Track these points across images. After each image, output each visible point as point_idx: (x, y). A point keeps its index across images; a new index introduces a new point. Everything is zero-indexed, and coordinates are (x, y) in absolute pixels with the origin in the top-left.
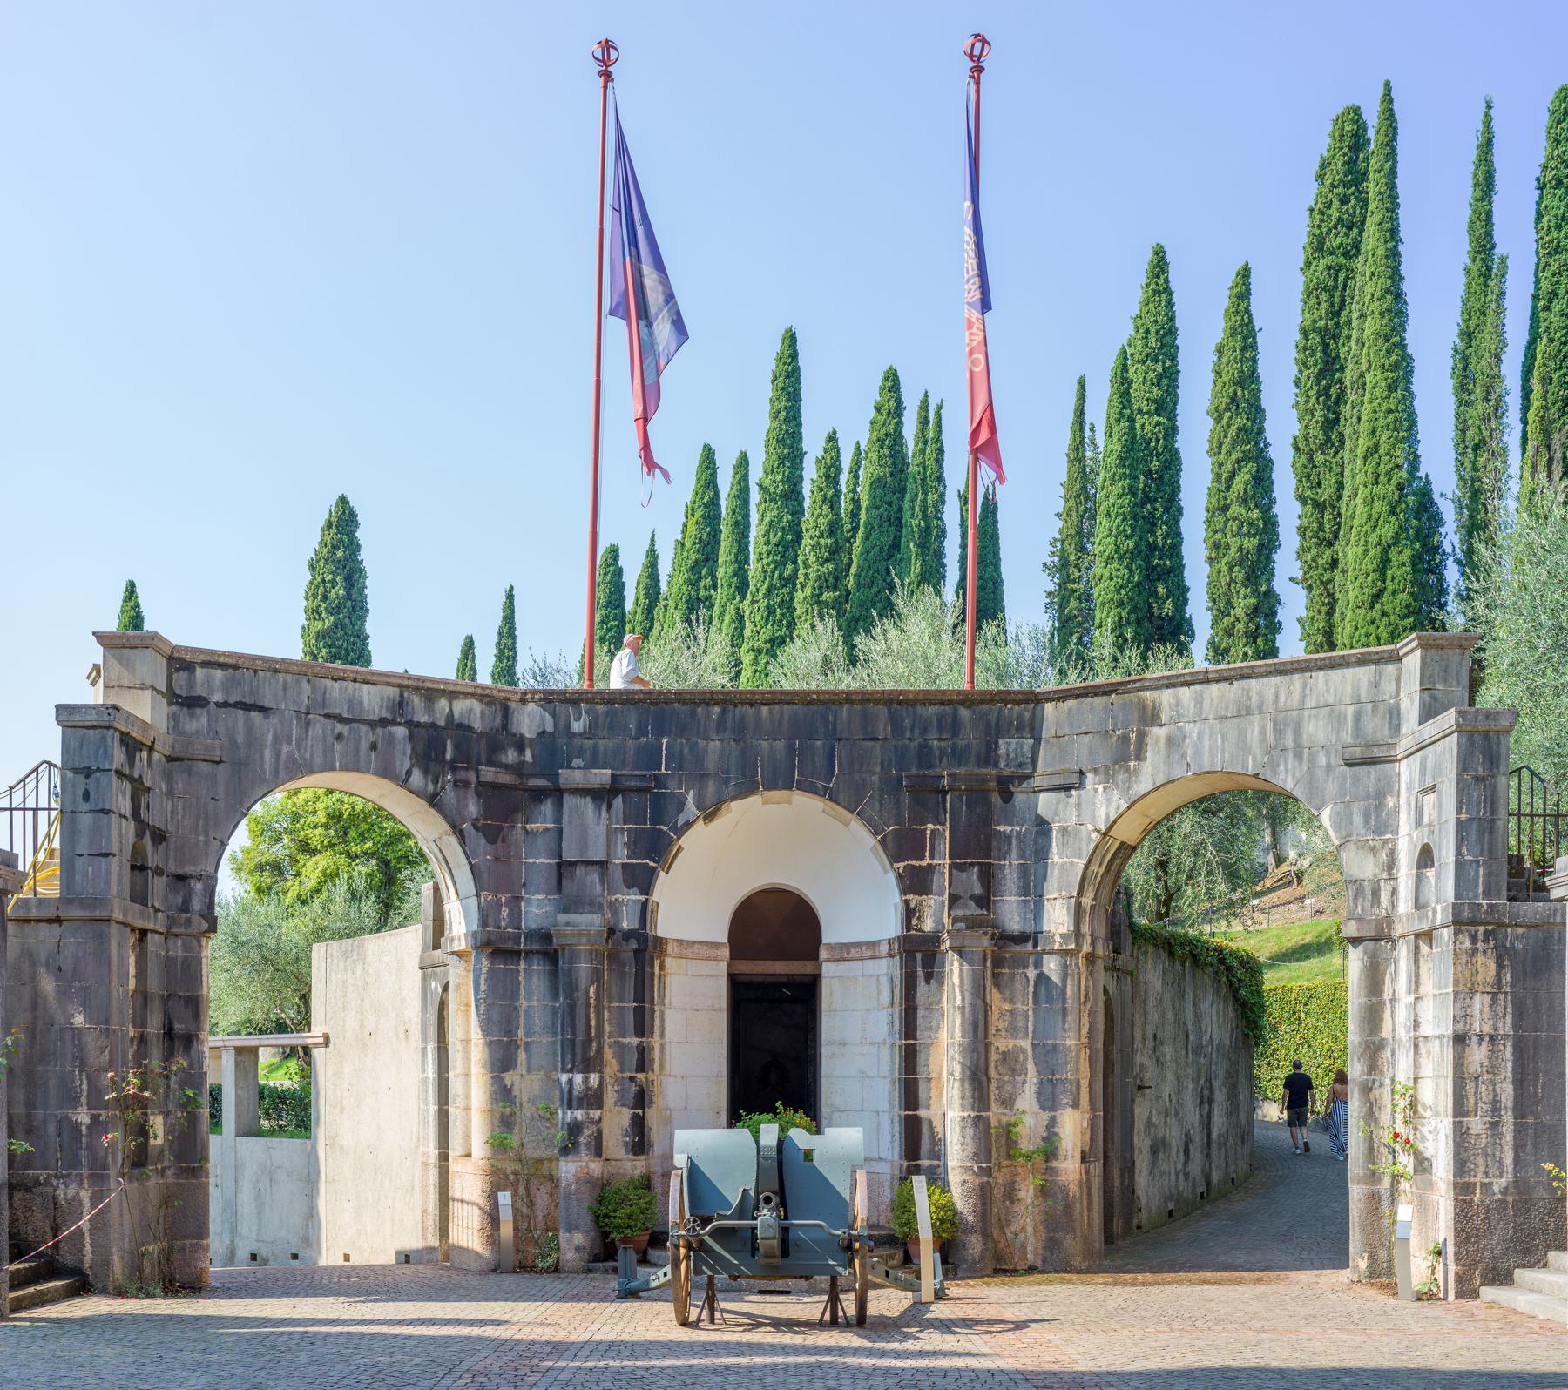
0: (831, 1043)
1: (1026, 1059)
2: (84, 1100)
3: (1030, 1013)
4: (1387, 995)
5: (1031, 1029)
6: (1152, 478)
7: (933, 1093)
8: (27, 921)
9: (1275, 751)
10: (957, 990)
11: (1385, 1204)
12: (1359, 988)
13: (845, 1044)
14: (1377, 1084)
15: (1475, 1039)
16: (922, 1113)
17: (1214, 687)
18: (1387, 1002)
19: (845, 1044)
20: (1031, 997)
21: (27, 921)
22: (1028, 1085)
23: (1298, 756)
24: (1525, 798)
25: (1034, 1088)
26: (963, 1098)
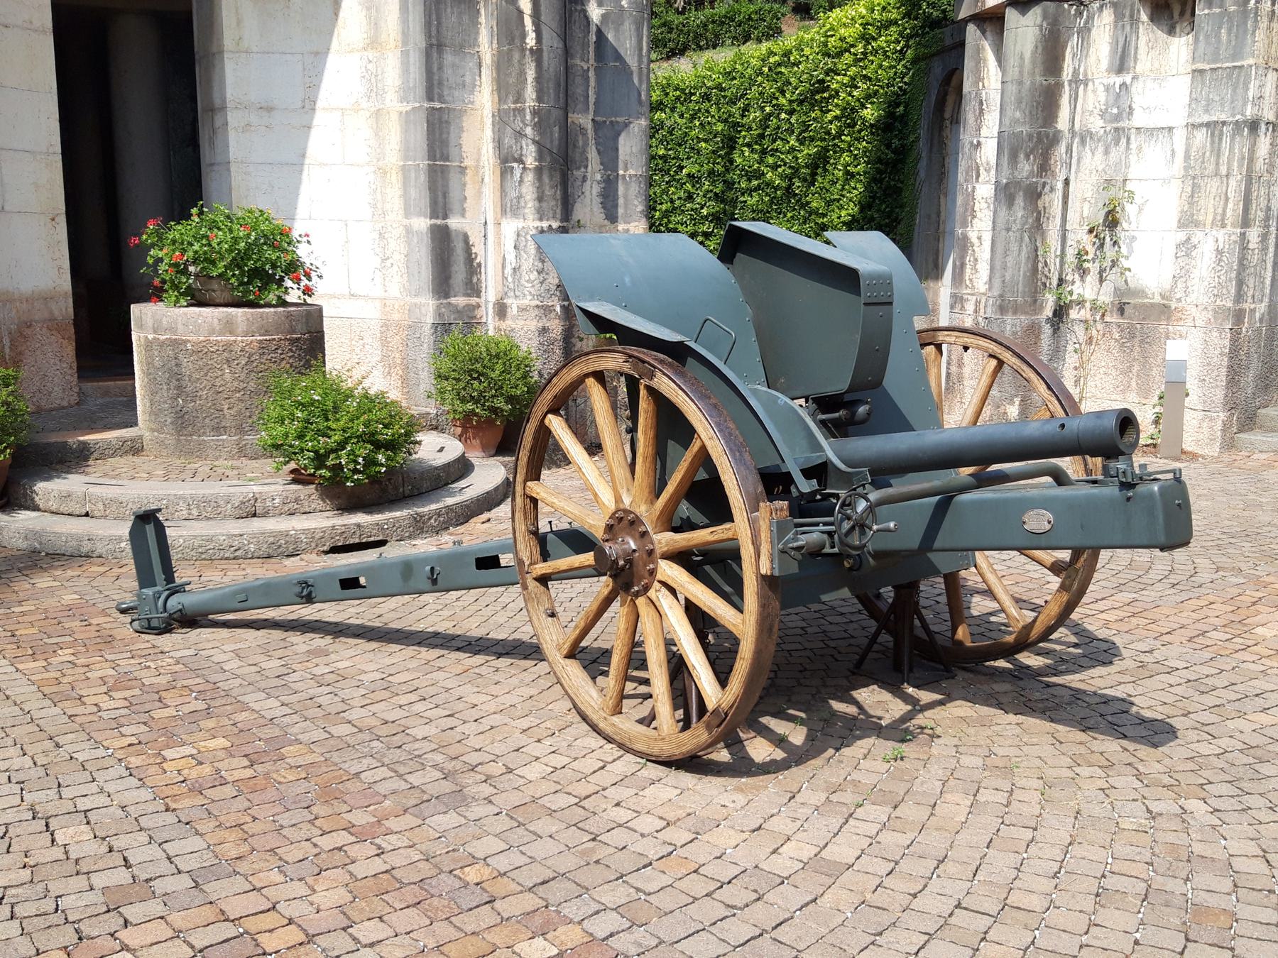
1: (586, 144)
3: (592, 74)
4: (1067, 74)
5: (592, 99)
7: (469, 192)
10: (528, 22)
12: (1033, 62)
13: (270, 109)
14: (1047, 188)
15: (1263, 127)
16: (454, 223)
18: (1066, 84)
19: (270, 109)
20: (592, 49)
22: (588, 182)
25: (596, 189)
26: (540, 199)
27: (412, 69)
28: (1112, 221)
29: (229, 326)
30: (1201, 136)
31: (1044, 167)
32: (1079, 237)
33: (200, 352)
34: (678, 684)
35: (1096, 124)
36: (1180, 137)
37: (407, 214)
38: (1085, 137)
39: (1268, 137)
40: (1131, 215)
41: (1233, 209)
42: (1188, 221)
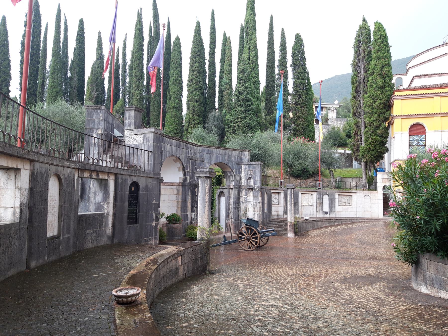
9: (228, 161)
23: (231, 162)
24: (143, 154)
27: (88, 188)
28: (246, 211)
30: (255, 203)
31: (239, 205)
35: (244, 201)
36: (252, 203)
38: (243, 202)
39: (36, 169)
42: (254, 211)
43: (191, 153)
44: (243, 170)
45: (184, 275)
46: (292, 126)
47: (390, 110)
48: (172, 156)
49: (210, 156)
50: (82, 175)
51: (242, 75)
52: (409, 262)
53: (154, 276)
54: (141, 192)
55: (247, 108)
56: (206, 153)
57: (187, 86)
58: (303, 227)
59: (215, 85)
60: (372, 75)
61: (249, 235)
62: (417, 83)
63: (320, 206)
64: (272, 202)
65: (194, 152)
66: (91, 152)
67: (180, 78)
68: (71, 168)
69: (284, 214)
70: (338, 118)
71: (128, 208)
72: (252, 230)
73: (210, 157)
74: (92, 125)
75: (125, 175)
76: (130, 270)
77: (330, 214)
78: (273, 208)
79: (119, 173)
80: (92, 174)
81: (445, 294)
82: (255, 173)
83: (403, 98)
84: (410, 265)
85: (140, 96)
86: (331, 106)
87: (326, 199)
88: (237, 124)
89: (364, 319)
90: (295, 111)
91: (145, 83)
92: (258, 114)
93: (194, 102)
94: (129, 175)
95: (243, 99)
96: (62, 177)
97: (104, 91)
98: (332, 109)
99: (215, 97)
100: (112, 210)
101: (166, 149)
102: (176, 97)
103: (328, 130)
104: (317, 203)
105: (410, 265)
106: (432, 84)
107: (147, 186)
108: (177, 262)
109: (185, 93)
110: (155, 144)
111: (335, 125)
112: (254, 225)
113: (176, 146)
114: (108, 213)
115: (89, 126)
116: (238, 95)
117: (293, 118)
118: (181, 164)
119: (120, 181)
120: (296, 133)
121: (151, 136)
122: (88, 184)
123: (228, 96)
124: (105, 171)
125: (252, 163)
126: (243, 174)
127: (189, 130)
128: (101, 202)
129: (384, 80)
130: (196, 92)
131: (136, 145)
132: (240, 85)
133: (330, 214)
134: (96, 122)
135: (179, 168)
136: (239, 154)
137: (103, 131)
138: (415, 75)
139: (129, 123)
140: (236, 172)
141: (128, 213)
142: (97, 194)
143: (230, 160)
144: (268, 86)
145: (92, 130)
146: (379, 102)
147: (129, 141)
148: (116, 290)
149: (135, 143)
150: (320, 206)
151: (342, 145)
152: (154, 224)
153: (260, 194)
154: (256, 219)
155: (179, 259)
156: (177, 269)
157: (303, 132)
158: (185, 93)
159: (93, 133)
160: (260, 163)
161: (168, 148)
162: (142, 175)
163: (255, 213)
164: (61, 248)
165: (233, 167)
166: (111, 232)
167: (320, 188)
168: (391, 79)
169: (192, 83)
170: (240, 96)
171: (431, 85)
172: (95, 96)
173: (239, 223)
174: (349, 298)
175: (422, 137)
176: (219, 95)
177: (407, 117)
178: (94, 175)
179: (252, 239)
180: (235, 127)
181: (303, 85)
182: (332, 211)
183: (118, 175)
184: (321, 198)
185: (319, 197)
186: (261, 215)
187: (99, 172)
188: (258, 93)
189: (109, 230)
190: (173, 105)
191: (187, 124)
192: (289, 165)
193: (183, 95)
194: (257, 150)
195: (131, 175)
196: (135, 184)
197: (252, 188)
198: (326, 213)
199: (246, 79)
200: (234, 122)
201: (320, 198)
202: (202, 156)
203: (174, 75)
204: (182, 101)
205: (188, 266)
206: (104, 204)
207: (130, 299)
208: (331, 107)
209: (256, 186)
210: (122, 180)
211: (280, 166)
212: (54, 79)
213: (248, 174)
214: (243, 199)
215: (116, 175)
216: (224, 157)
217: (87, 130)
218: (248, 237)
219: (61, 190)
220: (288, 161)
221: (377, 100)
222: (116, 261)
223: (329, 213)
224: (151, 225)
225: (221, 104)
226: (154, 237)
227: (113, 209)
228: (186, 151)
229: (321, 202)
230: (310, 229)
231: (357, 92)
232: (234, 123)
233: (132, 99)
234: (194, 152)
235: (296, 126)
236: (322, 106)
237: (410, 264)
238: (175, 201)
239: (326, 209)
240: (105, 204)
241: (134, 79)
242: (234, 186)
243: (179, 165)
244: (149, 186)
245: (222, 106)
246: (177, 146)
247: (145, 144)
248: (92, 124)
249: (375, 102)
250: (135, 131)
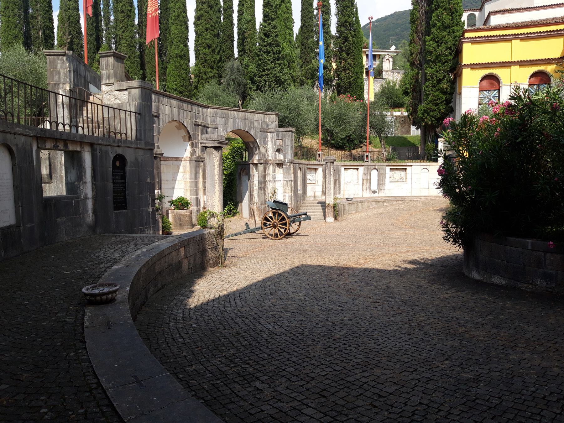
0: (163, 180)
2: (150, 204)
6: (506, 130)
8: (137, 148)
9: (250, 127)
11: (165, 217)
16: (198, 196)
17: (240, 113)
21: (137, 148)
23: (254, 129)
24: (128, 117)
28: (275, 192)
29: (187, 212)
31: (265, 185)
32: (270, 194)
33: (183, 215)
34: (452, 91)
35: (271, 180)
36: (282, 181)
37: (191, 195)
40: (277, 191)
41: (290, 191)
42: (285, 192)
43: (199, 117)
44: (269, 139)
45: (190, 269)
46: (335, 82)
47: (458, 57)
48: (173, 121)
49: (226, 121)
50: (44, 145)
51: (267, 10)
52: (460, 245)
53: (144, 271)
54: (128, 168)
55: (277, 56)
56: (220, 117)
57: (193, 26)
58: (344, 210)
59: (232, 24)
60: (436, 9)
61: (277, 222)
62: (495, 20)
63: (367, 183)
64: (308, 180)
65: (203, 116)
66: (60, 115)
67: (184, 14)
68: (26, 136)
69: (322, 195)
70: (394, 70)
71: (113, 189)
72: (280, 215)
73: (226, 123)
74: (56, 78)
75: (105, 145)
76: (114, 264)
77: (378, 193)
78: (309, 188)
79: (96, 142)
80: (58, 144)
81: (499, 279)
82: (285, 143)
83: (475, 41)
84: (460, 247)
85: (130, 39)
86: (386, 54)
87: (374, 173)
88: (264, 77)
89: (398, 309)
90: (340, 59)
91: (136, 22)
92: (291, 64)
93: (205, 48)
94: (111, 146)
95: (271, 43)
96: (14, 148)
97: (80, 33)
98: (387, 57)
99: (233, 41)
100: (91, 192)
101: (165, 111)
102: (179, 41)
103: (382, 85)
104: (363, 180)
105: (460, 247)
106: (511, 22)
107: (136, 159)
108: (179, 254)
109: (192, 35)
110: (143, 103)
111: (390, 78)
112: (282, 207)
113: (178, 108)
114: (86, 195)
115: (53, 80)
116: (264, 37)
117: (336, 69)
118: (187, 132)
119: (99, 154)
120: (340, 90)
121: (136, 92)
122: (59, 159)
123: (251, 39)
124: (75, 139)
125: (281, 129)
126: (270, 145)
127: (200, 87)
128: (75, 182)
129: (451, 16)
130: (207, 34)
131: (118, 104)
132: (266, 24)
133: (378, 193)
134: (62, 73)
135: (184, 137)
136: (264, 118)
137: (72, 86)
138: (491, 11)
139: (108, 75)
140: (260, 142)
141: (114, 196)
142: (69, 171)
143: (252, 126)
144: (304, 25)
145: (57, 85)
146: (445, 46)
147: (109, 100)
148: (87, 287)
149: (118, 102)
150: (367, 183)
151: (397, 105)
152: (151, 210)
153: (292, 171)
154: (287, 201)
155: (182, 251)
156: (180, 263)
157: (349, 88)
158: (192, 35)
159: (58, 89)
160: (291, 129)
161: (167, 110)
162: (128, 146)
163: (286, 194)
164: (22, 241)
165: (256, 135)
166: (93, 220)
167: (367, 160)
168: (461, 15)
169: (201, 20)
170: (266, 38)
171: (510, 24)
172: (69, 40)
173: (265, 207)
174: (385, 287)
175: (495, 93)
176: (239, 38)
177: (478, 67)
178: (61, 146)
179: (279, 225)
180: (260, 81)
181: (350, 24)
182: (381, 189)
183: (95, 146)
184: (369, 173)
185: (366, 172)
186: (293, 197)
187: (67, 142)
188: (291, 35)
189: (89, 217)
190: (176, 51)
191: (197, 79)
192: (328, 132)
193: (189, 37)
194: (288, 113)
195: (114, 146)
196: (120, 158)
197: (281, 162)
198: (374, 192)
199: (274, 15)
200: (260, 75)
201: (368, 173)
202: (214, 121)
203: (176, 10)
204: (188, 46)
205: (195, 259)
206: (79, 184)
207: (104, 297)
208: (386, 55)
209: (286, 160)
210: (102, 152)
211: (318, 133)
212: (9, 17)
213: (275, 144)
214: (269, 177)
215: (92, 145)
216: (243, 123)
217: (51, 85)
218: (275, 224)
219: (13, 165)
220: (328, 127)
221: (441, 43)
222: (97, 255)
223: (377, 192)
224: (147, 210)
225: (242, 51)
226: (151, 226)
227: (93, 191)
228: (192, 115)
229: (368, 178)
230: (353, 212)
231: (417, 33)
232: (260, 77)
233: (119, 44)
234: (203, 116)
235: (340, 81)
236: (374, 53)
237: (461, 246)
238: (181, 181)
239: (374, 186)
240: (81, 184)
241: (120, 16)
242: (259, 160)
243: (184, 134)
244: (140, 160)
245: (242, 53)
246: (179, 108)
247: (131, 103)
248: (57, 77)
249: (438, 46)
250: (116, 86)
